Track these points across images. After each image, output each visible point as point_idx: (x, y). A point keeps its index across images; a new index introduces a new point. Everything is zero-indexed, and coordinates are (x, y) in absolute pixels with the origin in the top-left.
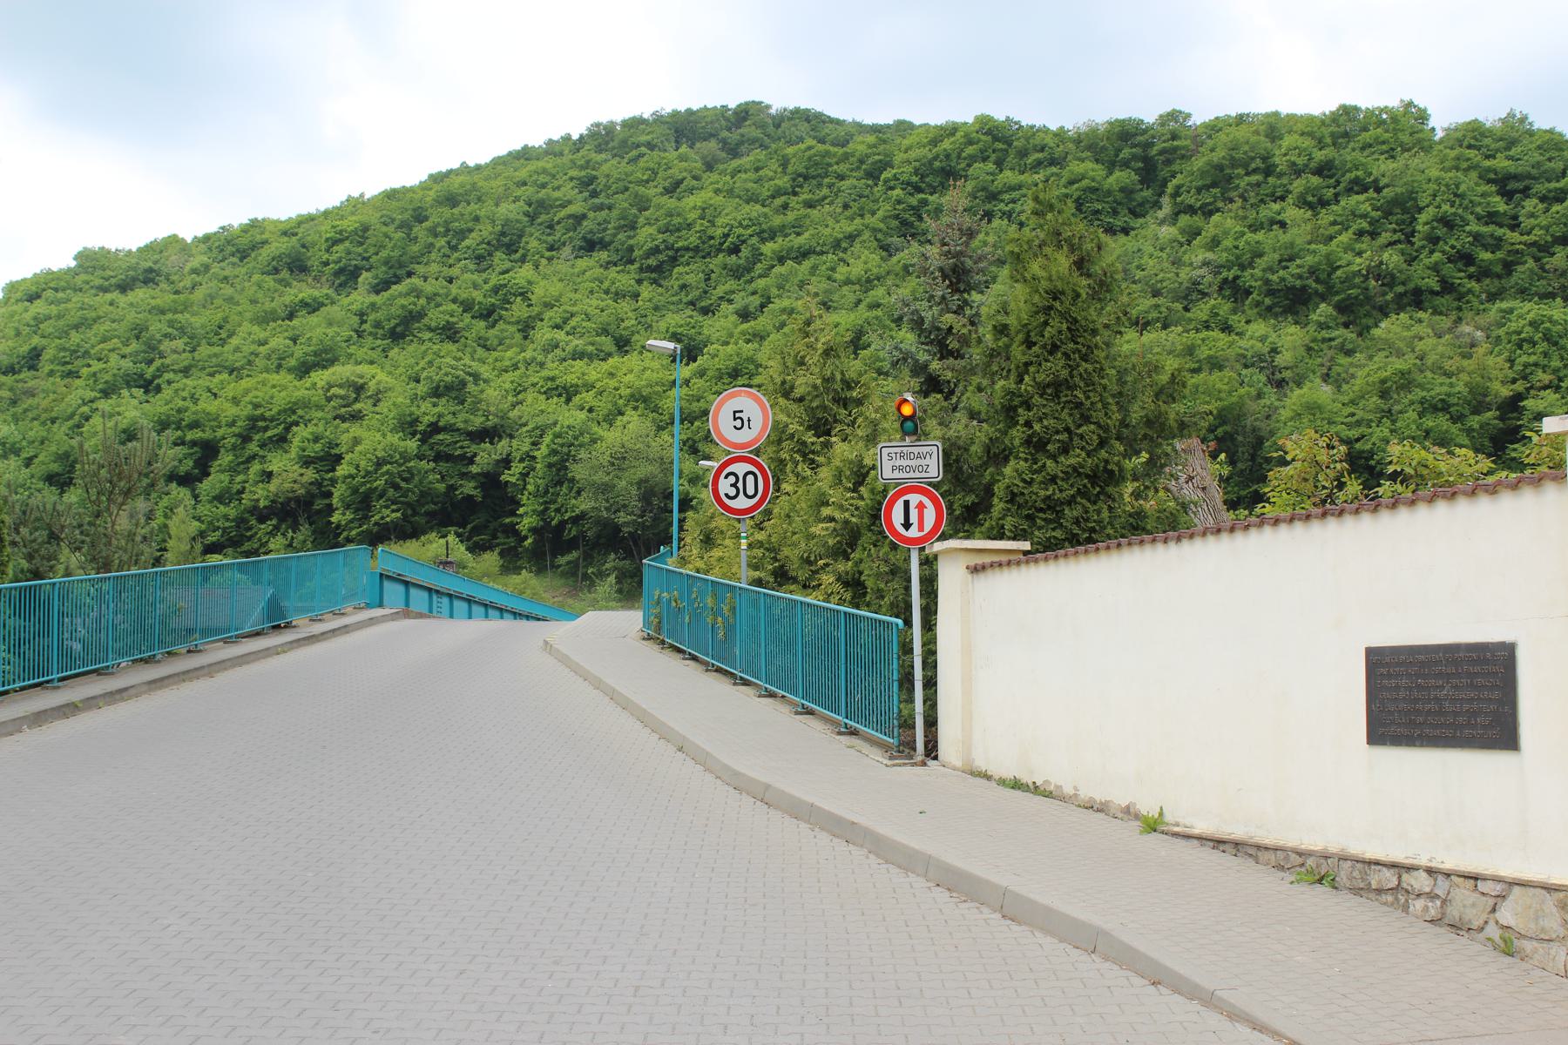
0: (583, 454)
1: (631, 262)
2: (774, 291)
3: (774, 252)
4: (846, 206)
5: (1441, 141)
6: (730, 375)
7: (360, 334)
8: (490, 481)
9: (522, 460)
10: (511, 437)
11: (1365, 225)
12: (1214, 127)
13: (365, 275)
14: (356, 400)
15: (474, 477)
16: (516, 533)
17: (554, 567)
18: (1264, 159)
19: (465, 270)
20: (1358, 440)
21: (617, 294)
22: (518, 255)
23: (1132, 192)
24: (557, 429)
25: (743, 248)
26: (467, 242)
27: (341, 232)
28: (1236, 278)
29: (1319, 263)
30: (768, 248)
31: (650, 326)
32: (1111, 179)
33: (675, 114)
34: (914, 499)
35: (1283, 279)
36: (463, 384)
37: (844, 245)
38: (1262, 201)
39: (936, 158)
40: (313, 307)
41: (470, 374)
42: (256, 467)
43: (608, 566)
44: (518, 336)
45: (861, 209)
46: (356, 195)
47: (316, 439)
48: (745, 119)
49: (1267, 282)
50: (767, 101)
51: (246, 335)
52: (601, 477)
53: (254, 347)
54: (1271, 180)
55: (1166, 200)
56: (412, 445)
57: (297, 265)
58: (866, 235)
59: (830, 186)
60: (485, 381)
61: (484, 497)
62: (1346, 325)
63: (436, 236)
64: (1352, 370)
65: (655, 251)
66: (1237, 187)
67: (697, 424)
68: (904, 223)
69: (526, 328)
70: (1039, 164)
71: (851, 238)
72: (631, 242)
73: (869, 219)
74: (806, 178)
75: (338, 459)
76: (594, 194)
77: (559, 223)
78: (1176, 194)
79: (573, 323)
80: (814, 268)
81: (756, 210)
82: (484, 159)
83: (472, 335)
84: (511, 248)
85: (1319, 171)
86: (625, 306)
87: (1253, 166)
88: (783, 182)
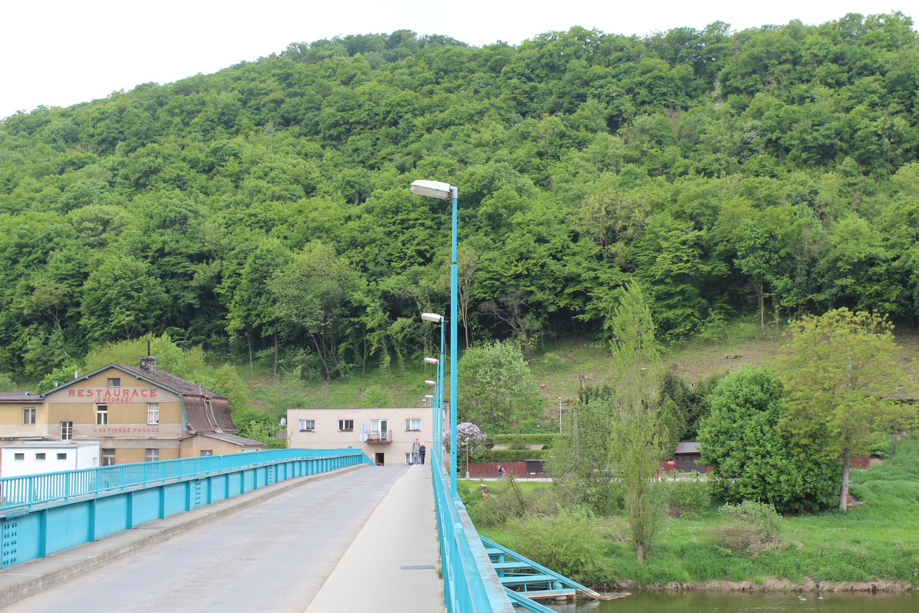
0: (278, 273)
1: (317, 133)
2: (424, 151)
3: (423, 124)
4: (476, 92)
6: (393, 212)
7: (112, 184)
8: (207, 294)
9: (230, 276)
10: (222, 259)
11: (875, 98)
12: (743, 37)
13: (120, 143)
14: (104, 231)
15: (193, 289)
16: (226, 334)
17: (256, 359)
18: (793, 53)
19: (194, 140)
20: (894, 259)
21: (306, 155)
22: (233, 129)
23: (689, 80)
24: (258, 252)
25: (400, 121)
26: (196, 120)
27: (103, 113)
28: (778, 138)
29: (843, 127)
30: (419, 121)
31: (331, 178)
32: (674, 71)
35: (816, 139)
36: (185, 218)
37: (476, 118)
38: (792, 83)
39: (542, 57)
40: (78, 165)
41: (190, 211)
42: (22, 282)
43: (298, 358)
44: (231, 185)
45: (488, 93)
46: (118, 90)
48: (398, 42)
49: (803, 141)
50: (413, 30)
51: (27, 183)
52: (293, 291)
53: (31, 194)
54: (798, 67)
55: (717, 84)
56: (143, 265)
57: (71, 138)
58: (492, 111)
59: (464, 78)
60: (203, 217)
61: (201, 304)
62: (866, 174)
63: (173, 115)
64: (877, 207)
65: (336, 124)
66: (773, 73)
67: (367, 249)
68: (520, 103)
69: (237, 179)
70: (620, 60)
71: (481, 113)
72: (317, 119)
73: (494, 100)
74: (446, 72)
75: (86, 275)
76: (290, 85)
77: (264, 106)
78: (725, 80)
79: (272, 174)
80: (454, 136)
81: (409, 94)
83: (196, 185)
84: (228, 124)
85: (835, 60)
86: (312, 164)
87: (784, 57)
88: (429, 75)
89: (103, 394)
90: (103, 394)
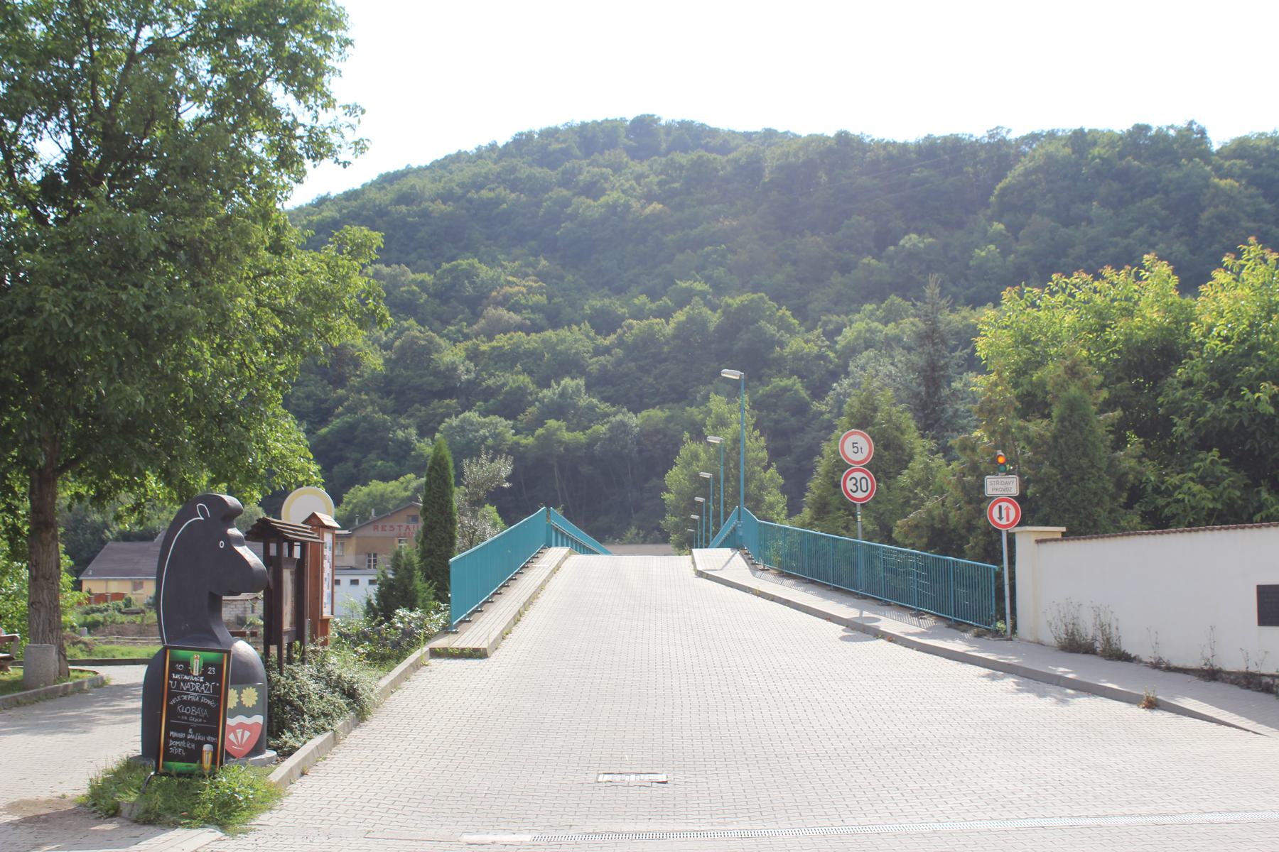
5: (1218, 152)
33: (584, 126)
34: (1004, 505)
47: (308, 397)
82: (426, 162)
89: (403, 529)
90: (403, 529)
